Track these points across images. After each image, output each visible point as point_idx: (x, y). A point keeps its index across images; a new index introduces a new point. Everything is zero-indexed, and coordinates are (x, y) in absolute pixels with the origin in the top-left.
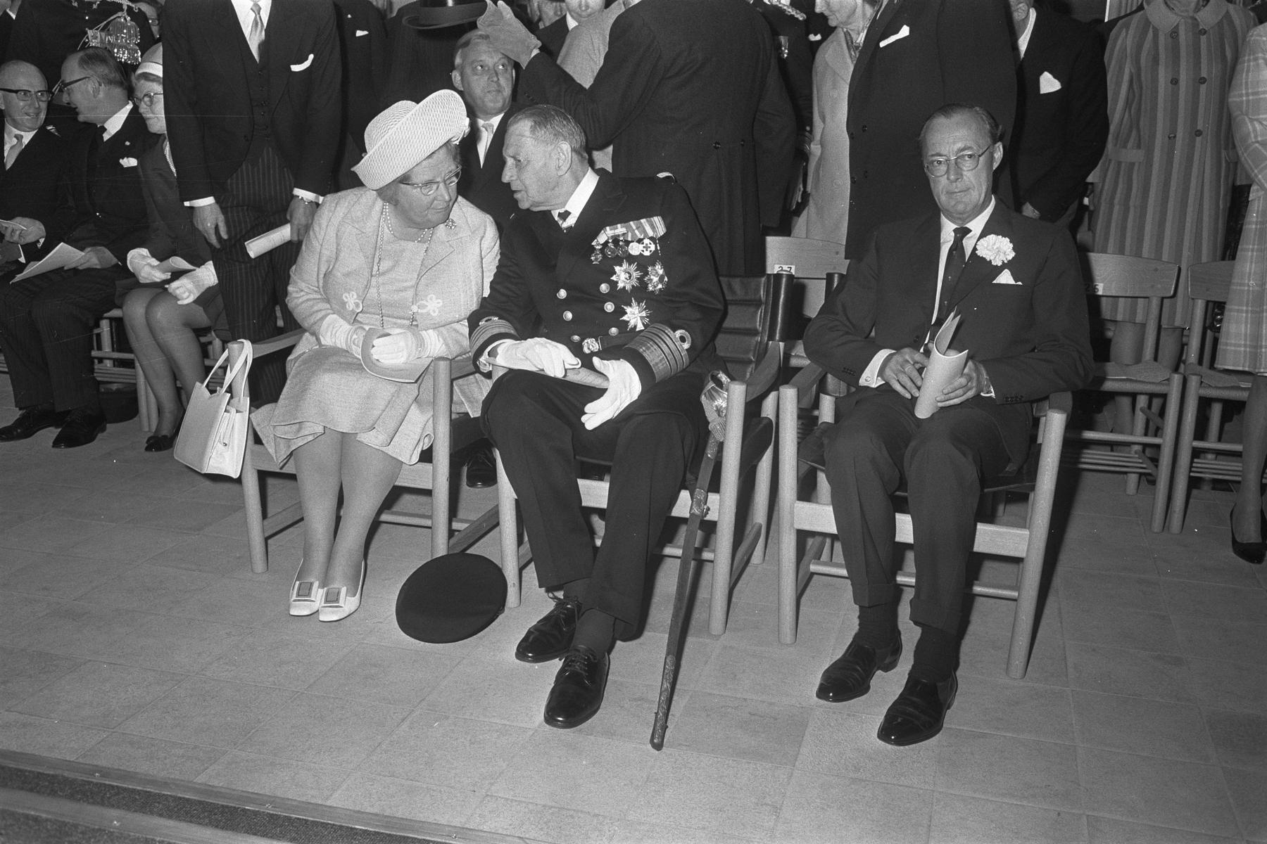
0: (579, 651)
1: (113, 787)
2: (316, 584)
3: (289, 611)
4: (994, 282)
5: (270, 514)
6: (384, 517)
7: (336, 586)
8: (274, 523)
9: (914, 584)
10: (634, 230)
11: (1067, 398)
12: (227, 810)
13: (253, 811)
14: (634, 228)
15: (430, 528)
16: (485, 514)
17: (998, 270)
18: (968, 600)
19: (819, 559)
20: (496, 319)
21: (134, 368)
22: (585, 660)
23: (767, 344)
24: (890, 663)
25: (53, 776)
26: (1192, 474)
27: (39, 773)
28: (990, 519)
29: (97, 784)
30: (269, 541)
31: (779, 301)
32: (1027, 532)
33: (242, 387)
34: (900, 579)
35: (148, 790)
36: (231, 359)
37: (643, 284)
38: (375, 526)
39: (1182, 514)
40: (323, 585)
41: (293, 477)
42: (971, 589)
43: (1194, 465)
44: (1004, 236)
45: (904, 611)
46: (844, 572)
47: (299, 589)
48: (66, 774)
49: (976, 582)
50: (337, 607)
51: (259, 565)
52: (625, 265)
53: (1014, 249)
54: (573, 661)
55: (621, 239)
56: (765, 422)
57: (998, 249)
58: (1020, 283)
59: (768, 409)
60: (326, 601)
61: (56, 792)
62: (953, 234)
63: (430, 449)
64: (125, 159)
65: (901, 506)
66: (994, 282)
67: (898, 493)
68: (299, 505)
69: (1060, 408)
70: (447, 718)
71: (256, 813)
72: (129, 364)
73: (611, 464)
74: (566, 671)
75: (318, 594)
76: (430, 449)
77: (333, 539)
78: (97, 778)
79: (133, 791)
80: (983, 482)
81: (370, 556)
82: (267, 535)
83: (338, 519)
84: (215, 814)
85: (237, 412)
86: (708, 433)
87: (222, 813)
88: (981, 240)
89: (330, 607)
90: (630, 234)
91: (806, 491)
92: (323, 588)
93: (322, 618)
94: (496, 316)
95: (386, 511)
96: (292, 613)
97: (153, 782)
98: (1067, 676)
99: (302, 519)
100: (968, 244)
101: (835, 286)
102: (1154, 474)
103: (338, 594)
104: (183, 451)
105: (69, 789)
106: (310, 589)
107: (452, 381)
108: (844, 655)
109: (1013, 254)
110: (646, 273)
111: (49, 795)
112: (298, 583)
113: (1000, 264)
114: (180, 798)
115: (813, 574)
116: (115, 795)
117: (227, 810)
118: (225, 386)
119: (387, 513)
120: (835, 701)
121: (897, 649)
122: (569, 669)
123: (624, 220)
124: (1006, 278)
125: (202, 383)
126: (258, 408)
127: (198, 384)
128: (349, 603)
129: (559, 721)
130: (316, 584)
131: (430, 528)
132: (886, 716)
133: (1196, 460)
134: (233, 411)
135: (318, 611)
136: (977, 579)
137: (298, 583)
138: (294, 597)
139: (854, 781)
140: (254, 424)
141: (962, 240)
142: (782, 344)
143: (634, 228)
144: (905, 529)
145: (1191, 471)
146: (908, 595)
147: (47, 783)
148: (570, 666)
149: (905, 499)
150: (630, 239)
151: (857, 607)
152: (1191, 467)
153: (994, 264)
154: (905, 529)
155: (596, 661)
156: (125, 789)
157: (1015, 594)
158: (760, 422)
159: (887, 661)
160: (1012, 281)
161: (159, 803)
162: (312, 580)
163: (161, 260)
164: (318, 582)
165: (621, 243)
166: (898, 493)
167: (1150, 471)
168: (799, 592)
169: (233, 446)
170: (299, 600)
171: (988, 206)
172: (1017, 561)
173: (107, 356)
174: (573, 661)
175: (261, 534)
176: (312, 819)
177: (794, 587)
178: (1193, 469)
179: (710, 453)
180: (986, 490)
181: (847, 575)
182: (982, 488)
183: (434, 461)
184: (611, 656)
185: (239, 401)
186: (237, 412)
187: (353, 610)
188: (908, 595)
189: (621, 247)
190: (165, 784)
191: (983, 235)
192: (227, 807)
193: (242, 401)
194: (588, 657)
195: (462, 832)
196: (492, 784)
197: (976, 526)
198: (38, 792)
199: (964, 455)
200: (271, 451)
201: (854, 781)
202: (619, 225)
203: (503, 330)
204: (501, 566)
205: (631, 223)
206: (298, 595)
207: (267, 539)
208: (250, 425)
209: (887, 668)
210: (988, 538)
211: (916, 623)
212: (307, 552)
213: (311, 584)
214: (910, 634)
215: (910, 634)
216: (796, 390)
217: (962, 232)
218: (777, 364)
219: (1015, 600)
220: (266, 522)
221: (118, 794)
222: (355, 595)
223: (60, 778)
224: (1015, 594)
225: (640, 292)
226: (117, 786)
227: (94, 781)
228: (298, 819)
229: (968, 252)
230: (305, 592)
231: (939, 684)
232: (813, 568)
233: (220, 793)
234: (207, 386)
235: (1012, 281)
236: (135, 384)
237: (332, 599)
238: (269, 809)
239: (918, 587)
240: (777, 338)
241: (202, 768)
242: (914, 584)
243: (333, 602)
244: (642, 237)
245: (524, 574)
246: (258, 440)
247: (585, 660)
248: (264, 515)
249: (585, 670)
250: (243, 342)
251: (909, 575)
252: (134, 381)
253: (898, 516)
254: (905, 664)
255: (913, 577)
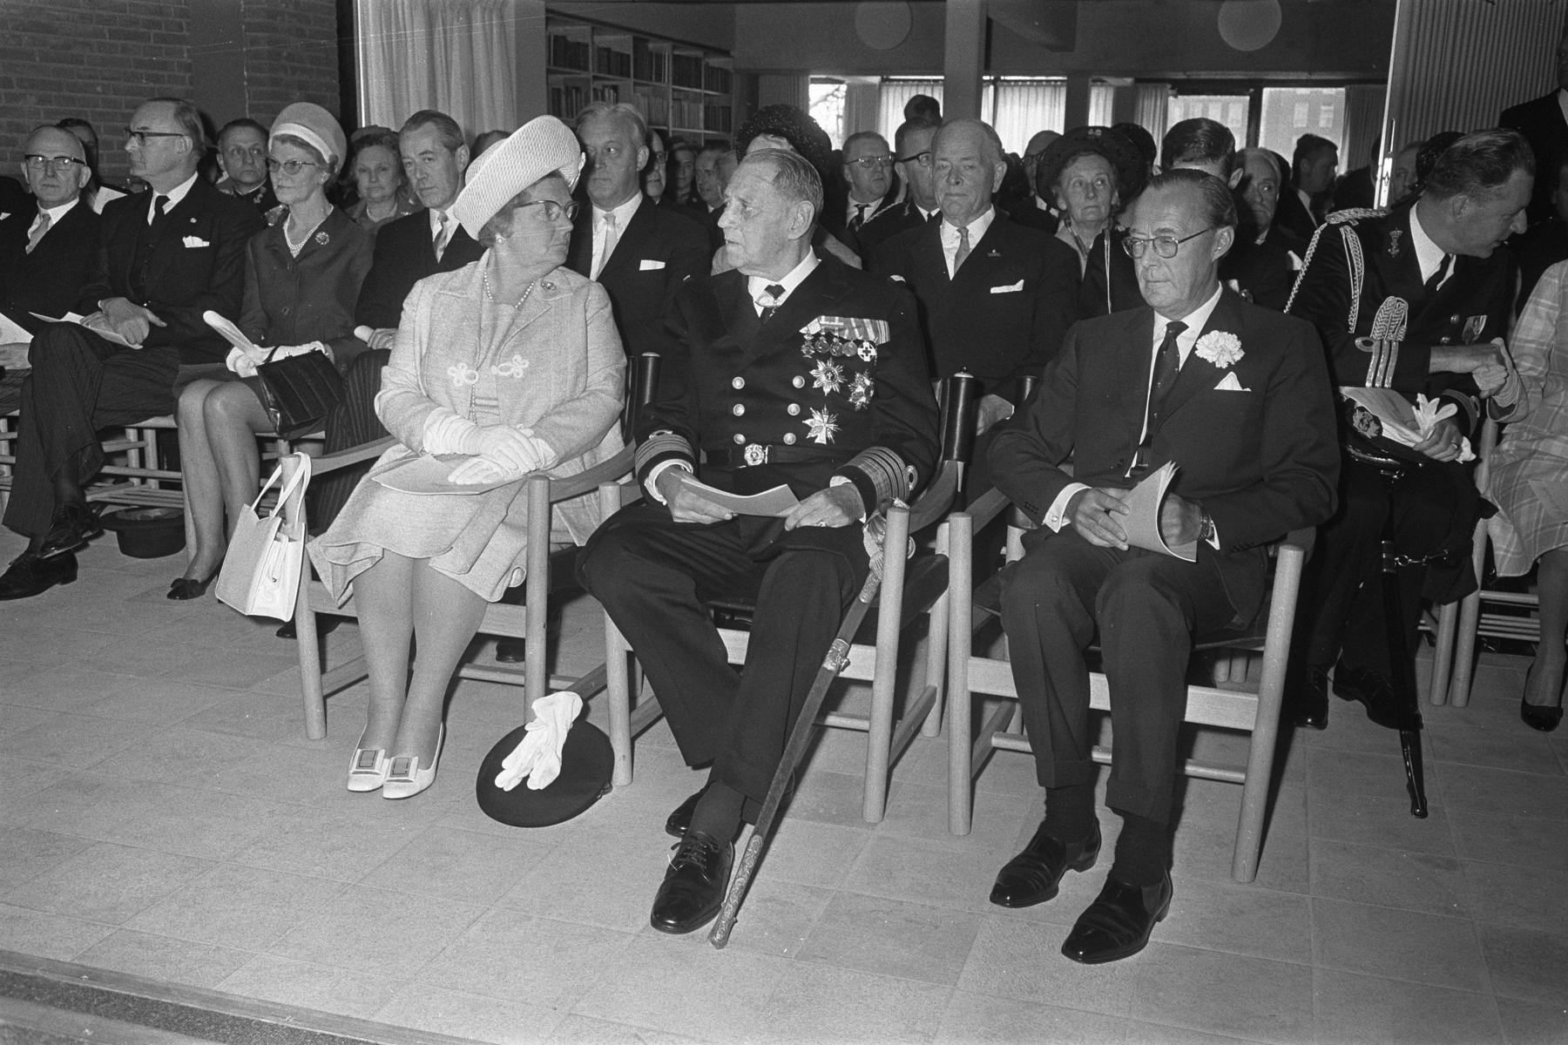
0: (696, 838)
1: (102, 992)
2: (382, 753)
3: (347, 785)
4: (1217, 388)
5: (329, 668)
6: (464, 672)
7: (404, 755)
8: (332, 680)
9: (1110, 762)
10: (853, 328)
11: (1310, 534)
12: (238, 1023)
13: (270, 1025)
14: (854, 325)
15: (522, 686)
16: (594, 671)
17: (1222, 373)
18: (1179, 784)
19: (1005, 731)
20: (670, 433)
21: (181, 489)
22: (704, 849)
23: (943, 464)
24: (1086, 861)
25: (31, 977)
26: (1479, 633)
27: (15, 974)
28: (1207, 681)
29: (83, 989)
30: (329, 701)
31: (957, 411)
32: (1255, 698)
33: (297, 511)
34: (1097, 756)
35: (146, 996)
36: (285, 479)
37: (845, 390)
38: (454, 682)
39: (1468, 682)
40: (388, 756)
41: (354, 620)
42: (1184, 769)
43: (1482, 621)
44: (1231, 332)
45: (1101, 792)
46: (1027, 747)
47: (360, 759)
48: (48, 976)
49: (1189, 760)
50: (406, 781)
51: (316, 729)
52: (821, 366)
53: (1243, 347)
54: (689, 851)
55: (836, 334)
56: (939, 560)
57: (1222, 349)
58: (1248, 390)
59: (942, 545)
60: (393, 774)
61: (33, 998)
62: (1165, 329)
63: (523, 588)
64: (190, 237)
65: (1095, 665)
66: (1217, 388)
67: (1092, 647)
68: (362, 659)
69: (1296, 545)
70: (530, 918)
71: (273, 1027)
72: (176, 485)
73: (753, 609)
74: (680, 863)
75: (383, 765)
76: (523, 588)
77: (404, 696)
78: (84, 982)
79: (126, 997)
80: (1194, 637)
81: (450, 717)
82: (326, 691)
83: (410, 673)
84: (223, 1027)
85: (290, 540)
86: (868, 570)
87: (232, 1026)
88: (1203, 337)
89: (397, 781)
90: (847, 331)
91: (981, 645)
92: (390, 758)
93: (387, 794)
94: (670, 429)
95: (467, 664)
96: (350, 788)
97: (151, 987)
98: (1307, 880)
99: (366, 677)
100: (1184, 345)
101: (1027, 392)
102: (1434, 631)
103: (408, 766)
104: (224, 588)
105: (49, 993)
106: (374, 759)
107: (551, 504)
108: (1027, 850)
109: (1242, 354)
110: (852, 380)
111: (25, 999)
112: (359, 751)
113: (1225, 366)
114: (183, 1007)
115: (995, 749)
116: (103, 1003)
117: (238, 1023)
118: (276, 510)
119: (468, 668)
120: (1011, 906)
121: (1093, 845)
122: (684, 860)
123: (844, 314)
124: (1230, 383)
125: (251, 505)
126: (316, 535)
127: (246, 506)
128: (420, 777)
129: (670, 924)
130: (382, 753)
131: (522, 686)
132: (1075, 926)
133: (1484, 616)
134: (285, 538)
135: (382, 787)
136: (1190, 757)
137: (359, 751)
138: (354, 769)
139: (1028, 1005)
140: (311, 556)
141: (1176, 337)
142: (960, 465)
143: (854, 325)
144: (1099, 693)
145: (1478, 629)
146: (1105, 774)
147: (23, 986)
148: (685, 857)
149: (1098, 654)
150: (845, 338)
151: (1043, 790)
152: (1478, 623)
153: (1218, 366)
154: (1099, 693)
155: (717, 852)
156: (117, 996)
157: (1240, 777)
158: (933, 561)
159: (1080, 858)
160: (1238, 388)
161: (156, 1012)
162: (374, 748)
163: (1394, 386)
164: (383, 751)
165: (835, 340)
166: (1092, 647)
167: (1428, 628)
168: (892, 762)
169: (284, 583)
170: (361, 773)
171: (1212, 295)
172: (1247, 734)
173: (149, 474)
174: (689, 851)
175: (319, 692)
176: (341, 1035)
177: (886, 749)
178: (1482, 621)
179: (865, 597)
180: (1197, 647)
181: (1030, 749)
182: (1194, 642)
183: (528, 603)
184: (736, 846)
185: (293, 527)
186: (290, 540)
187: (430, 783)
188: (1105, 774)
189: (835, 344)
190: (167, 990)
191: (1206, 330)
192: (239, 1019)
193: (296, 527)
194: (708, 848)
195: (392, 1032)
196: (577, 1001)
197: (1186, 689)
198: (11, 996)
199: (1168, 598)
200: (329, 588)
201: (1028, 1005)
202: (837, 318)
203: (675, 448)
204: (607, 734)
205: (852, 319)
206: (359, 766)
207: (325, 698)
208: (306, 561)
209: (1081, 867)
210: (1200, 705)
211: (1116, 811)
212: (372, 713)
213: (376, 753)
214: (1110, 826)
215: (1110, 826)
216: (969, 518)
217: (1177, 328)
218: (952, 490)
219: (1242, 784)
220: (325, 676)
221: (107, 1001)
222: (428, 768)
223: (39, 980)
224: (1240, 777)
225: (837, 404)
226: (108, 992)
227: (81, 984)
228: (324, 1035)
229: (1183, 356)
230: (367, 764)
231: (1145, 890)
232: (995, 742)
233: (232, 1001)
234: (257, 510)
235: (1238, 388)
236: (182, 510)
237: (399, 772)
238: (290, 1022)
239: (1114, 765)
240: (955, 457)
241: (223, 974)
242: (1110, 762)
243: (400, 775)
244: (860, 338)
245: (636, 745)
246: (315, 577)
247: (704, 849)
248: (323, 670)
249: (703, 863)
250: (299, 456)
251: (1105, 751)
252: (181, 506)
253: (1093, 677)
254: (1104, 861)
255: (1108, 752)
